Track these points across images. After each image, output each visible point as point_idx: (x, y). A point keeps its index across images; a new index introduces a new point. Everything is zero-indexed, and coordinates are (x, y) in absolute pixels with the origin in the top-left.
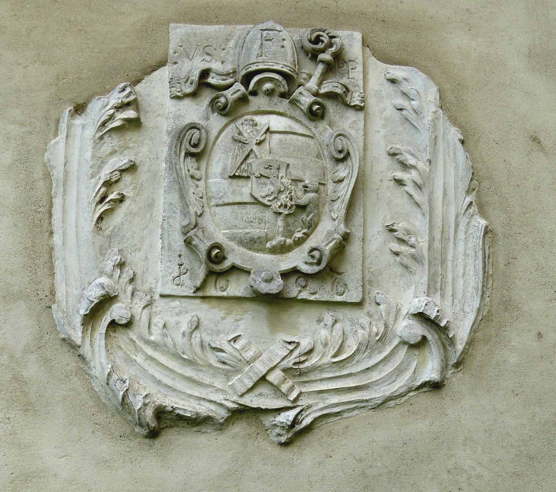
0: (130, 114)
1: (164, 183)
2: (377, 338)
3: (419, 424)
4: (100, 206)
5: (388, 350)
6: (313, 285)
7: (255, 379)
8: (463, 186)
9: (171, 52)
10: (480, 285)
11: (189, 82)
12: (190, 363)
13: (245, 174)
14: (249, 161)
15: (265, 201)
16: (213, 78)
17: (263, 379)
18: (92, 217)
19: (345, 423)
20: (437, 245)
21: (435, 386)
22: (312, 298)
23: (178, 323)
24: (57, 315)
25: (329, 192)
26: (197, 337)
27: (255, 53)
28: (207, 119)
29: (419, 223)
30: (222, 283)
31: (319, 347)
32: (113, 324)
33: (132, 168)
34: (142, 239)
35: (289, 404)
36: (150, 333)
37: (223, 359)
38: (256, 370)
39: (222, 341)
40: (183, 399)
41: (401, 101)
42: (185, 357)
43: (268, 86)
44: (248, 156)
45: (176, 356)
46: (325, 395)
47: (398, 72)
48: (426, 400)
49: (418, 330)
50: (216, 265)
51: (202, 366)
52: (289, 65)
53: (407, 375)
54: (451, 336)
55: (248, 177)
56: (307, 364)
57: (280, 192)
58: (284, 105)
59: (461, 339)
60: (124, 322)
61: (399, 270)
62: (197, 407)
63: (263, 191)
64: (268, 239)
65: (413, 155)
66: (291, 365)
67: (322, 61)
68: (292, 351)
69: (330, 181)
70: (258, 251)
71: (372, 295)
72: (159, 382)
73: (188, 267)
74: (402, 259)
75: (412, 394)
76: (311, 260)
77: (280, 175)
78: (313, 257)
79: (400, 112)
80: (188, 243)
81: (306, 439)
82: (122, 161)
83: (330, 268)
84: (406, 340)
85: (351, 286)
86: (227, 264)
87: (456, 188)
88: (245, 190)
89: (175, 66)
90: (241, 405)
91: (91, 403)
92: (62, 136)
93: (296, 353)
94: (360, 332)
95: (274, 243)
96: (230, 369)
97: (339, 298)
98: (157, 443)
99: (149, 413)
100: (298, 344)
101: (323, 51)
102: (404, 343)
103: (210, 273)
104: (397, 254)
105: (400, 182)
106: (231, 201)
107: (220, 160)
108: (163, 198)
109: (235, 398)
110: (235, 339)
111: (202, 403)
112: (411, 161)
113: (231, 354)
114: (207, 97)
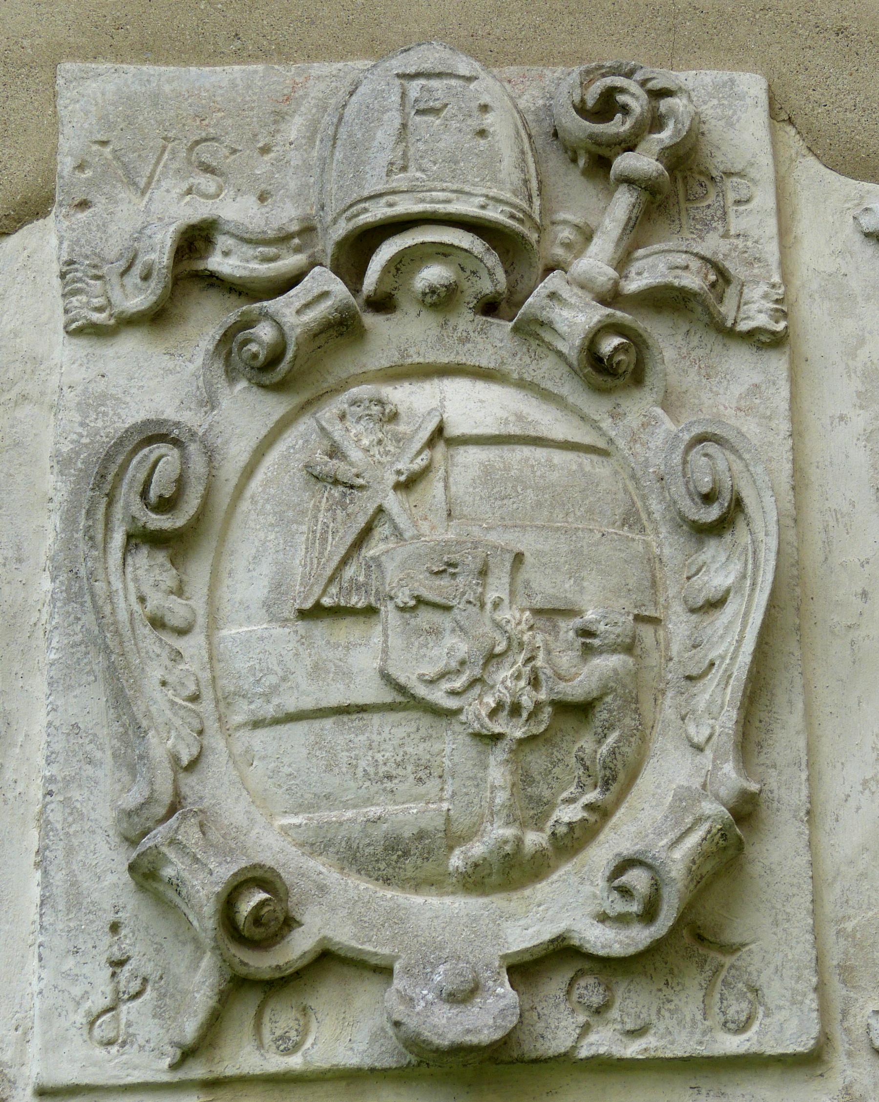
1: (48, 653)
6: (633, 1001)
9: (66, 164)
11: (137, 270)
13: (357, 601)
15: (438, 696)
16: (226, 254)
22: (633, 1050)
28: (210, 402)
30: (282, 1019)
43: (433, 274)
52: (508, 196)
55: (371, 611)
57: (492, 658)
58: (495, 341)
64: (453, 839)
69: (677, 607)
70: (418, 885)
73: (148, 969)
77: (491, 596)
80: (145, 874)
85: (775, 991)
86: (300, 945)
88: (360, 660)
89: (83, 216)
95: (478, 849)
97: (732, 1044)
106: (308, 703)
107: (265, 552)
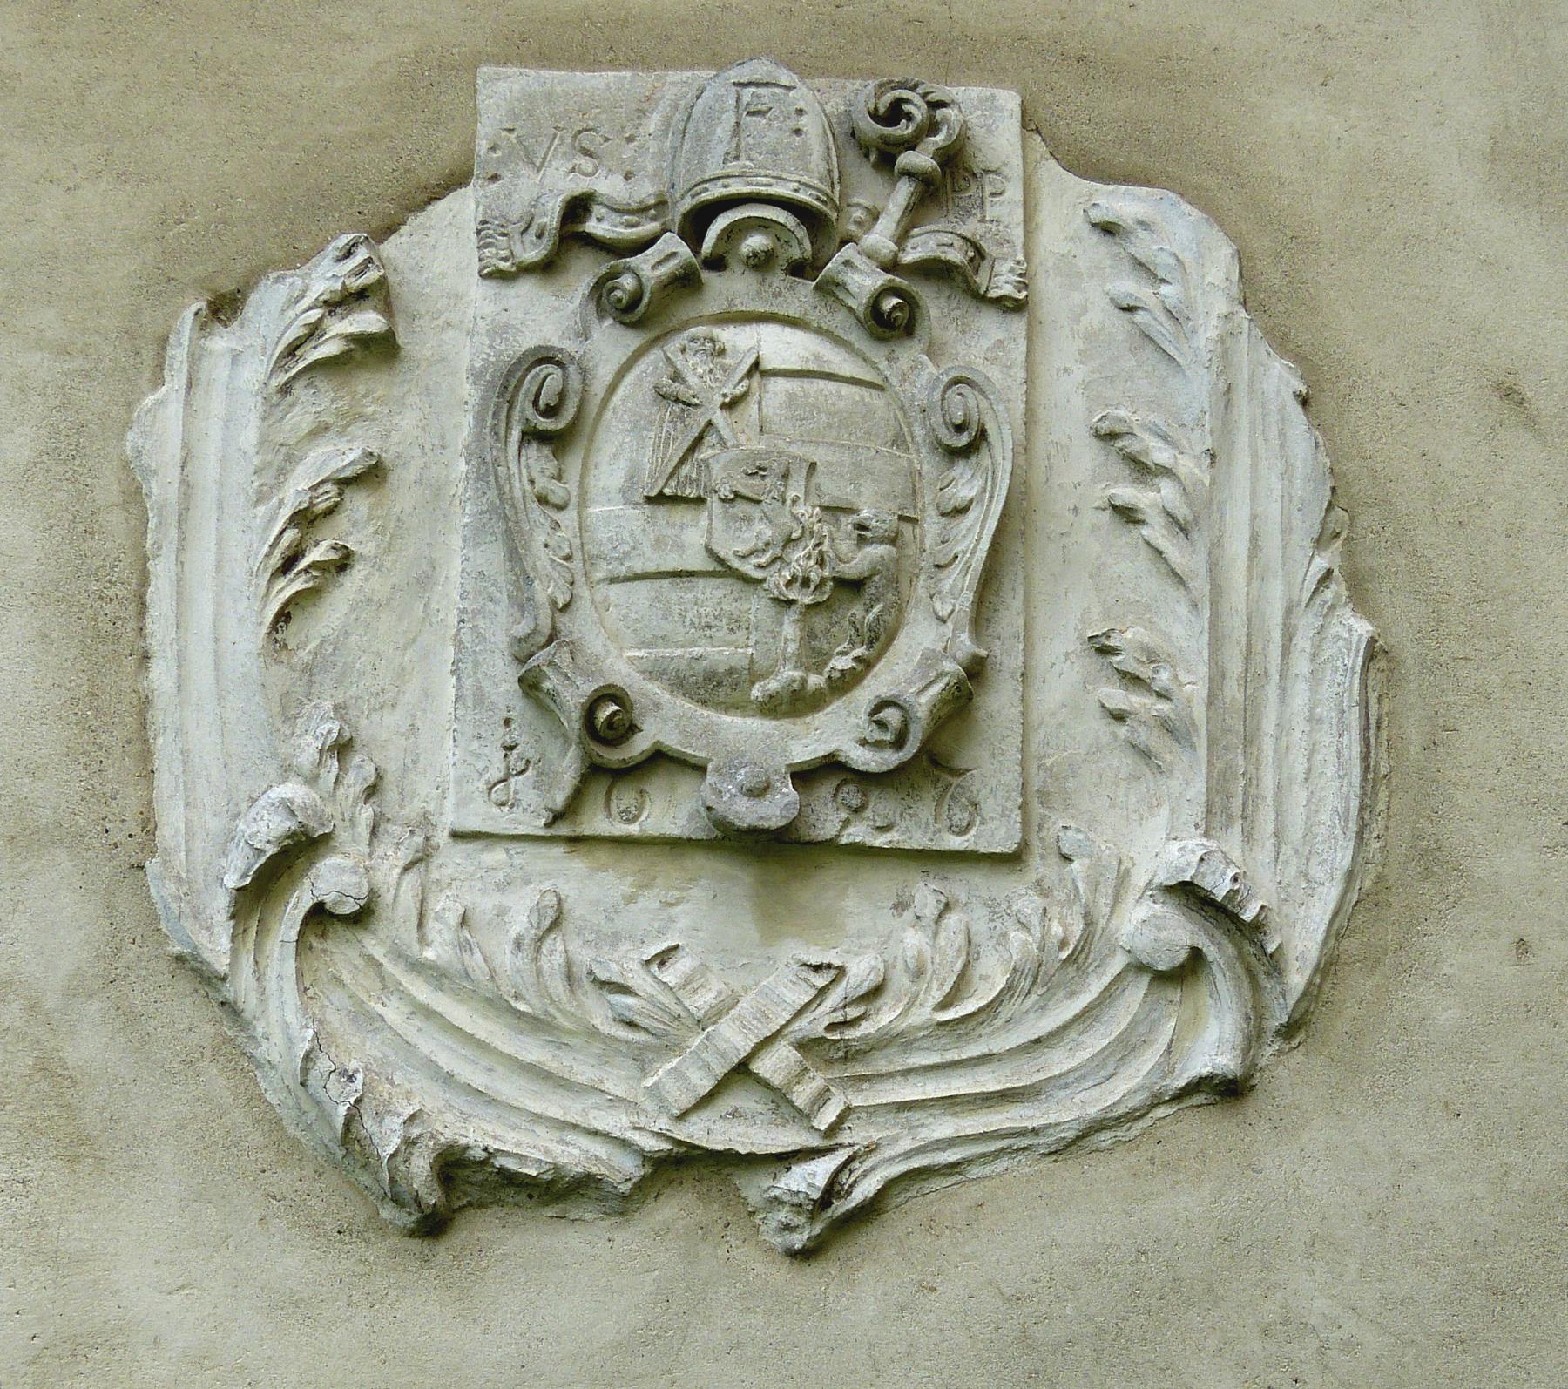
0: (368, 321)
1: (463, 517)
2: (1064, 955)
3: (1182, 1196)
4: (281, 582)
5: (1094, 988)
6: (882, 806)
7: (720, 1070)
8: (1307, 524)
9: (482, 146)
10: (1354, 804)
11: (533, 230)
12: (537, 1024)
13: (690, 492)
14: (701, 455)
15: (748, 568)
16: (599, 220)
17: (742, 1070)
18: (261, 613)
19: (974, 1193)
20: (1232, 691)
21: (1227, 1091)
22: (880, 841)
23: (501, 912)
24: (162, 889)
25: (928, 543)
26: (554, 953)
27: (720, 150)
28: (585, 335)
29: (1180, 630)
30: (625, 798)
31: (900, 981)
32: (319, 915)
33: (372, 475)
34: (402, 674)
35: (815, 1142)
36: (423, 940)
37: (629, 1015)
38: (722, 1046)
39: (625, 964)
40: (515, 1128)
41: (1130, 286)
42: (522, 1007)
43: (756, 242)
44: (699, 440)
45: (497, 1005)
46: (917, 1116)
47: (1123, 203)
48: (1200, 1128)
49: (1179, 932)
50: (610, 749)
51: (570, 1033)
52: (815, 182)
53: (1149, 1059)
54: (1271, 948)
55: (700, 501)
56: (865, 1028)
57: (789, 541)
58: (800, 297)
59: (1301, 957)
60: (349, 908)
61: (1126, 763)
62: (557, 1149)
63: (740, 539)
64: (755, 676)
65: (1164, 438)
66: (819, 1030)
67: (908, 173)
68: (822, 992)
69: (932, 511)
70: (727, 708)
71: (1050, 833)
72: (448, 1079)
73: (530, 754)
74: (1133, 730)
75: (1161, 1112)
76: (877, 735)
77: (791, 494)
78: (882, 725)
79: (1127, 315)
80: (530, 685)
81: (862, 1241)
82: (344, 455)
83: (931, 756)
84: (1145, 959)
85: (989, 806)
86: (640, 745)
87: (1287, 530)
88: (691, 538)
89: (494, 186)
90: (679, 1143)
91: (257, 1138)
92: (174, 383)
93: (835, 997)
94: (1017, 936)
95: (773, 685)
96: (650, 1040)
97: (955, 843)
98: (444, 1250)
99: (421, 1166)
100: (841, 970)
101: (911, 144)
102: (1138, 967)
103: (593, 772)
104: (1119, 717)
105: (1127, 515)
106: (651, 567)
107: (621, 453)
108: (461, 559)
109: (663, 1124)
110: (663, 958)
111: (571, 1137)
112: (1160, 454)
113: (651, 1000)
114: (583, 273)
